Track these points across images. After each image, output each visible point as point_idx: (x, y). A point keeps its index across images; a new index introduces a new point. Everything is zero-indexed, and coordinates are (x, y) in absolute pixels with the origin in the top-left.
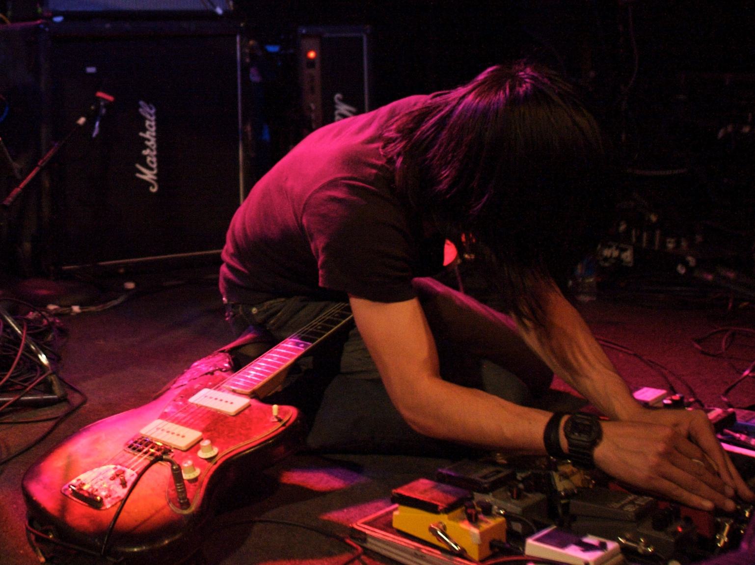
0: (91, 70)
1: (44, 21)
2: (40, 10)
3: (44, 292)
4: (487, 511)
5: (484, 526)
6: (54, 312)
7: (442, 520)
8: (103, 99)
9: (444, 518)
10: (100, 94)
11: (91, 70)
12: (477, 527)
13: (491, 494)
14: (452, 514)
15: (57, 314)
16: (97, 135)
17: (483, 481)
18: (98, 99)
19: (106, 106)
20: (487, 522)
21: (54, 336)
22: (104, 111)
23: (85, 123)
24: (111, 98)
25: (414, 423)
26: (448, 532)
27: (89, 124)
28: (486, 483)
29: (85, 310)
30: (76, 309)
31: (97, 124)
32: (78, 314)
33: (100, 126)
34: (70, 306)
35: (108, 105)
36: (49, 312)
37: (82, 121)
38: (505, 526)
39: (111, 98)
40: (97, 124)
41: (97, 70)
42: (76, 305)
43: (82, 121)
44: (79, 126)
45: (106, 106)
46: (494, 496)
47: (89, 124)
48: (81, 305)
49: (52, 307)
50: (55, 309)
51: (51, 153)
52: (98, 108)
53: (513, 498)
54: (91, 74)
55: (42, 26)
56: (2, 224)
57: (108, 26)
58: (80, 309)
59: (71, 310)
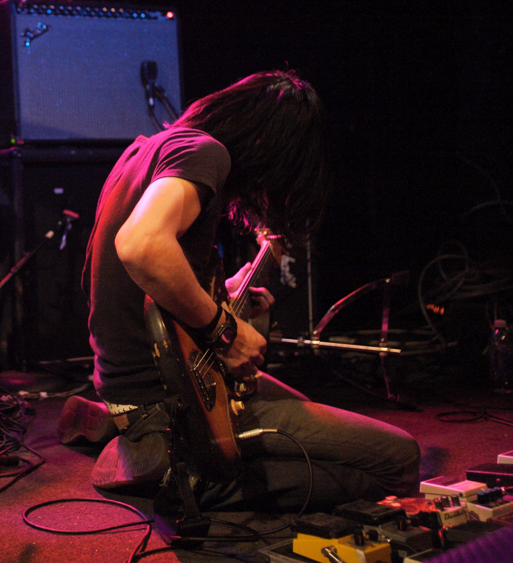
0: (59, 191)
1: (17, 148)
2: (13, 141)
3: (18, 382)
4: (374, 537)
5: (369, 550)
6: (24, 397)
7: (333, 544)
8: (69, 216)
9: (334, 542)
10: (67, 212)
11: (59, 191)
12: (363, 549)
13: (380, 526)
14: (342, 539)
15: (27, 399)
16: (64, 248)
17: (374, 515)
18: (65, 216)
19: (72, 222)
20: (372, 546)
21: (21, 413)
22: (70, 226)
23: (54, 237)
24: (76, 215)
25: (440, 517)
26: (338, 554)
27: (57, 238)
28: (376, 517)
29: (52, 396)
30: (44, 394)
31: (64, 238)
32: (45, 399)
33: (67, 239)
34: (38, 392)
35: (74, 222)
36: (19, 396)
37: (50, 234)
38: (390, 551)
39: (76, 215)
40: (64, 238)
41: (64, 191)
42: (43, 391)
43: (50, 234)
44: (48, 239)
45: (72, 222)
46: (382, 528)
47: (57, 238)
48: (48, 391)
49: (22, 393)
50: (25, 395)
51: (23, 261)
52: (65, 224)
53: (400, 530)
54: (59, 195)
55: (15, 153)
56: (4, 398)
57: (73, 152)
58: (48, 395)
59: (39, 395)
